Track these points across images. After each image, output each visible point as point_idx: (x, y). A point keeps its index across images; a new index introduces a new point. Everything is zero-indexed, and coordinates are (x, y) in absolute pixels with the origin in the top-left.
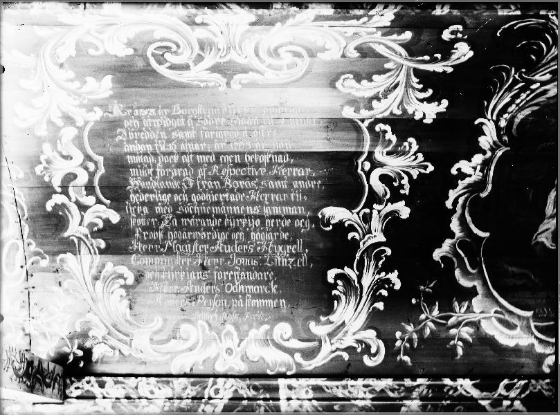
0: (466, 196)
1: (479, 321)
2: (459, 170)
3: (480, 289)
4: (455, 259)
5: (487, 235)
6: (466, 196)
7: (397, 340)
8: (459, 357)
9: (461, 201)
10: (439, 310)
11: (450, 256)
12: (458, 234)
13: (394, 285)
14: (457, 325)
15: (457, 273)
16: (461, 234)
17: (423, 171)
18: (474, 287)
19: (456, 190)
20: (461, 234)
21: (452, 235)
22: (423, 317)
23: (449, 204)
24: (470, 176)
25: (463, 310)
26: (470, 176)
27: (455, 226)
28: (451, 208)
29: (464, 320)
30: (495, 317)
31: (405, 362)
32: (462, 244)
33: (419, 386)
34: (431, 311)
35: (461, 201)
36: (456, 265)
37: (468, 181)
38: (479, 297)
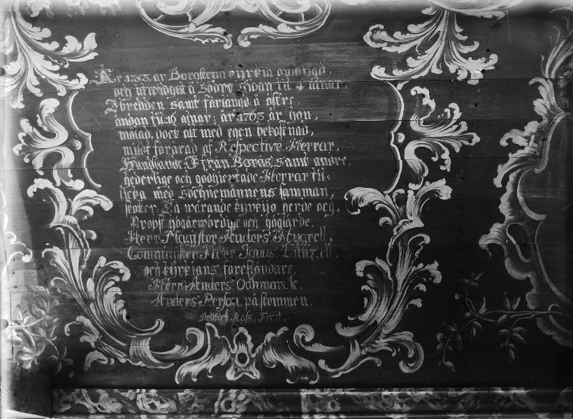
0: (518, 171)
1: (534, 320)
2: (509, 141)
3: (533, 281)
4: (504, 247)
5: (543, 217)
6: (518, 171)
7: (438, 343)
8: (511, 361)
9: (512, 178)
10: (486, 307)
11: (499, 243)
12: (508, 217)
13: (433, 278)
14: (509, 324)
15: (507, 263)
16: (512, 217)
17: (467, 143)
18: (528, 279)
19: (506, 165)
20: (512, 217)
21: (501, 218)
22: (468, 314)
23: (498, 182)
24: (523, 148)
25: (515, 307)
26: (523, 148)
27: (504, 207)
28: (501, 186)
29: (517, 317)
30: (554, 315)
31: (448, 368)
32: (514, 229)
33: (464, 396)
34: (478, 308)
35: (512, 178)
36: (506, 253)
37: (520, 153)
38: (534, 291)
